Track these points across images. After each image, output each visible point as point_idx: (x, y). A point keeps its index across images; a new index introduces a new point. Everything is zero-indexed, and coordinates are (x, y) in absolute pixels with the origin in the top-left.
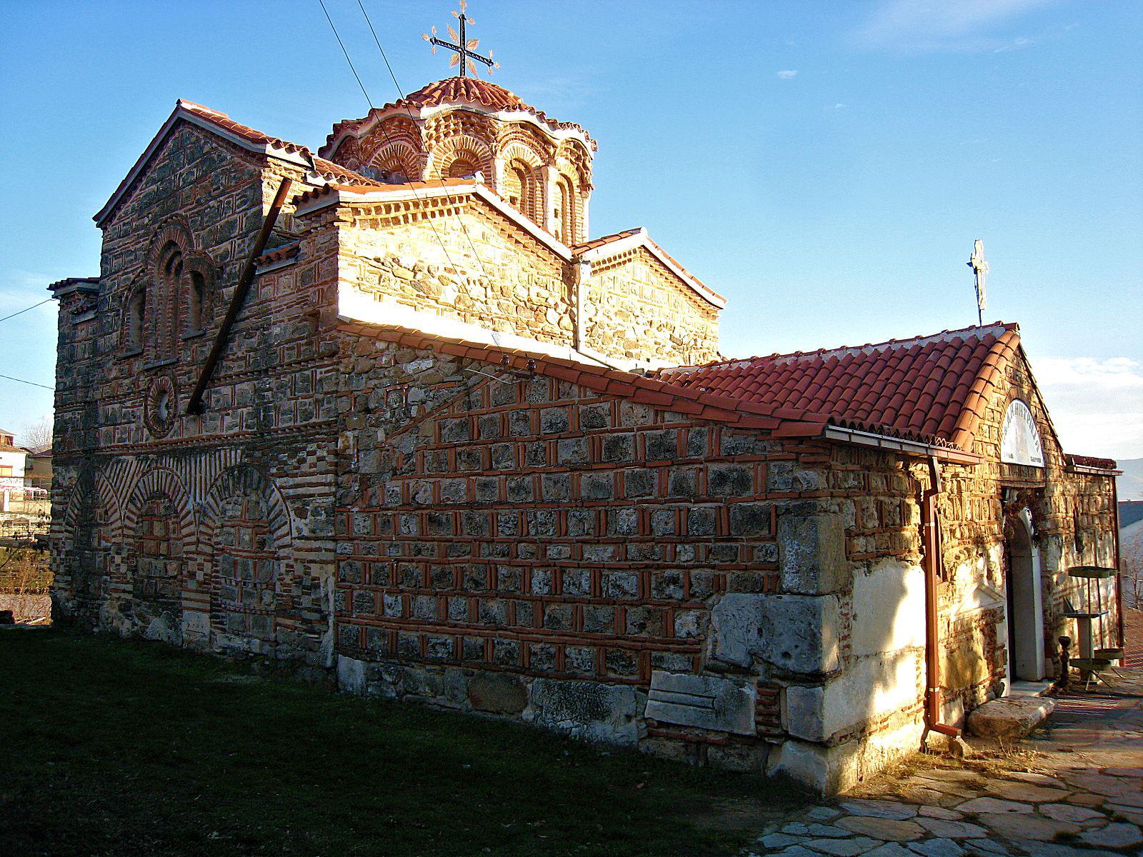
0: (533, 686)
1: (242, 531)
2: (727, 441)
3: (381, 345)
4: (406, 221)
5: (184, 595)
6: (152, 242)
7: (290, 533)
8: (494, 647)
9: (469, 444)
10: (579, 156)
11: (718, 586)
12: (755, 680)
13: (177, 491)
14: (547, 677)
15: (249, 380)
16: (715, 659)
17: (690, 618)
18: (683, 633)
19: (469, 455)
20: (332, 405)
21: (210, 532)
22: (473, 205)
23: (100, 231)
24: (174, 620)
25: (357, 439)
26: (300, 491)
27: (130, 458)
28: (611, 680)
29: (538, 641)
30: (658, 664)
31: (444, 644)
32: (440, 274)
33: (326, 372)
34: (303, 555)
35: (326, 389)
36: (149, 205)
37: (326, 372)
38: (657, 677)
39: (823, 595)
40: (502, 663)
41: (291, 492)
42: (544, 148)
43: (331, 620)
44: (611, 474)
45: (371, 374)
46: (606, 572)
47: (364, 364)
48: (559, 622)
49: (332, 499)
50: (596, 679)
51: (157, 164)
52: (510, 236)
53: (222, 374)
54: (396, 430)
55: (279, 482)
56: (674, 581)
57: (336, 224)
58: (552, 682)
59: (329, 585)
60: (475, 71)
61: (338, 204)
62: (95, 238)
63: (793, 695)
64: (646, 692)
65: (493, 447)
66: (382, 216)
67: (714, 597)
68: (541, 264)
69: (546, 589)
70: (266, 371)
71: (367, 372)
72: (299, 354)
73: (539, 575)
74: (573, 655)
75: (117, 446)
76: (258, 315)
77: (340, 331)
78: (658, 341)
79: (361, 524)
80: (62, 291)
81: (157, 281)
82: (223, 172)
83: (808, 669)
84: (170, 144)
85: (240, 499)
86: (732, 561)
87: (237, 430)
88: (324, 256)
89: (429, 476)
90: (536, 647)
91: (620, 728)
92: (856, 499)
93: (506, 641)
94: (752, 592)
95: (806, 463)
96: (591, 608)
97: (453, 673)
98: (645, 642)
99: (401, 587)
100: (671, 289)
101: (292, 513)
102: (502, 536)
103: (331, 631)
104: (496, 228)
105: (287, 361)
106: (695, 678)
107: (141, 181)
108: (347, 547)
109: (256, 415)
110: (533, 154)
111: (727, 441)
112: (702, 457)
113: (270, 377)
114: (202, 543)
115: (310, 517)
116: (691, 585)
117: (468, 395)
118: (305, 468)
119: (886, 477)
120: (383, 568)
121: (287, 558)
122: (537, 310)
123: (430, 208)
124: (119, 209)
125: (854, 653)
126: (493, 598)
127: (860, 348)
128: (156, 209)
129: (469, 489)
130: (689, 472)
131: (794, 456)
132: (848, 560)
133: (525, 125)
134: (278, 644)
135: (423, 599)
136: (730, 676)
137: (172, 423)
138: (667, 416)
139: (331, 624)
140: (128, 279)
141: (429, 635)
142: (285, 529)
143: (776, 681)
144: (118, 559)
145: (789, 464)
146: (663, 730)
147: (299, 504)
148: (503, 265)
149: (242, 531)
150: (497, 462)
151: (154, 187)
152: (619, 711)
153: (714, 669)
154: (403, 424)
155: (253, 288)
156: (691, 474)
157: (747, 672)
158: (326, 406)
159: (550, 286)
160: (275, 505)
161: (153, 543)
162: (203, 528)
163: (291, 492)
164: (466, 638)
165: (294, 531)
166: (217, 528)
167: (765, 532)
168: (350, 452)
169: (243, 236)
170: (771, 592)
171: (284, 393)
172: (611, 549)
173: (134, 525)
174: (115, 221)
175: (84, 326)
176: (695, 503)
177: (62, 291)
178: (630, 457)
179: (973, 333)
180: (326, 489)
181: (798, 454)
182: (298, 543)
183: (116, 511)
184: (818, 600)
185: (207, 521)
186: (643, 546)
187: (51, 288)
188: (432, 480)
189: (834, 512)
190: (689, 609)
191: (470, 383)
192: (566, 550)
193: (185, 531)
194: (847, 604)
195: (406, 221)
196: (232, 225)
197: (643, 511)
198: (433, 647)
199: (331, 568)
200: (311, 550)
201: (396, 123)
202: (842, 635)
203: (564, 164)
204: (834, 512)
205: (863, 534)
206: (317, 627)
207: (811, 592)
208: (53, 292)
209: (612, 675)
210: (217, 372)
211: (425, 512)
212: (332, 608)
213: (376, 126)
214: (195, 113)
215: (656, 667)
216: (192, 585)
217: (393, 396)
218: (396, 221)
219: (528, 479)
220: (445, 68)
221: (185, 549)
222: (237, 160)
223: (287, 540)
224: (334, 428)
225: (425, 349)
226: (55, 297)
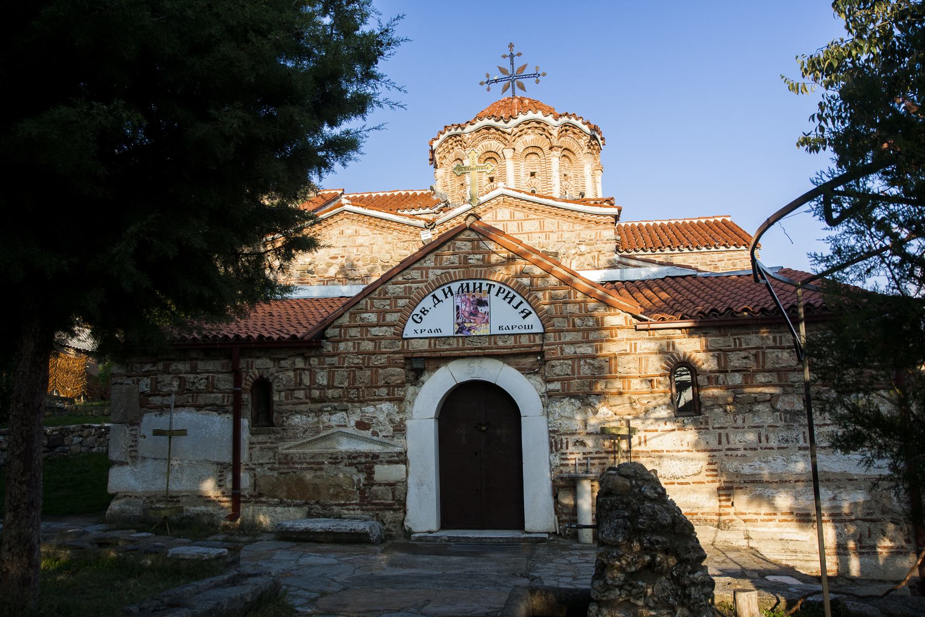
148: (371, 244)
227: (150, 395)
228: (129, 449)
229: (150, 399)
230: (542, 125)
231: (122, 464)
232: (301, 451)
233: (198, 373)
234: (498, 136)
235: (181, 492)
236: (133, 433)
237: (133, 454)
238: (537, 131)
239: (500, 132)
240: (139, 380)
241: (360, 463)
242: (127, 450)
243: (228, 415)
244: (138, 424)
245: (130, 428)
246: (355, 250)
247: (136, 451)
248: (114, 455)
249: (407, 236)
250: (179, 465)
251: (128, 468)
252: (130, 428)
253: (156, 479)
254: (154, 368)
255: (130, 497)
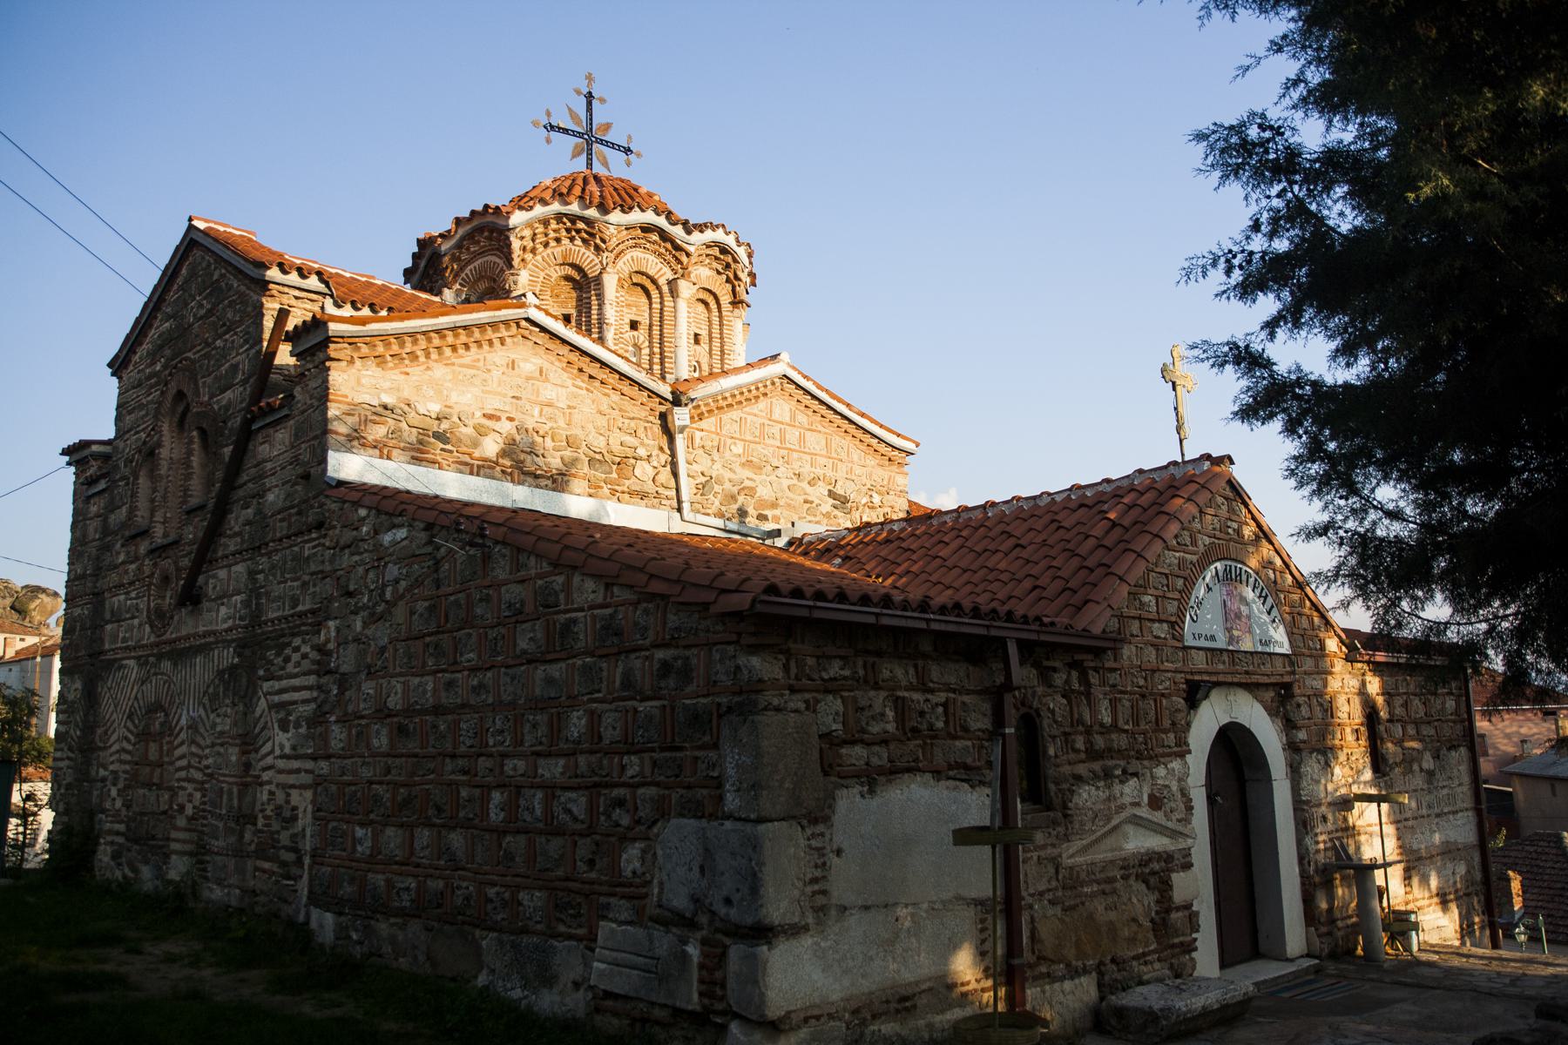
0: (488, 941)
1: (230, 750)
2: (673, 620)
3: (363, 512)
4: (428, 356)
5: (174, 835)
6: (163, 393)
7: (272, 752)
8: (453, 892)
9: (437, 633)
10: (728, 266)
11: (662, 812)
12: (699, 935)
13: (171, 703)
14: (500, 931)
15: (244, 561)
16: (660, 906)
17: (635, 851)
18: (628, 873)
19: (437, 646)
20: (318, 589)
21: (200, 752)
22: (526, 333)
23: (115, 380)
24: (161, 868)
25: (338, 630)
26: (286, 697)
27: (132, 663)
28: (560, 935)
29: (494, 884)
30: (603, 913)
31: (407, 889)
32: (476, 421)
33: (314, 547)
34: (282, 778)
35: (313, 568)
36: (161, 347)
37: (314, 547)
38: (605, 928)
39: (771, 821)
40: (459, 914)
41: (276, 698)
42: (674, 256)
43: (307, 861)
44: (563, 665)
45: (352, 548)
46: (558, 792)
47: (349, 535)
48: (513, 859)
49: (313, 706)
50: (544, 934)
51: (172, 296)
52: (581, 370)
53: (220, 554)
54: (374, 618)
55: (266, 686)
56: (620, 803)
57: (328, 364)
58: (505, 937)
59: (305, 821)
60: (615, 167)
61: (328, 340)
62: (109, 389)
63: (736, 952)
64: (593, 950)
65: (458, 634)
66: (408, 350)
67: (659, 824)
68: (627, 405)
69: (502, 815)
70: (259, 547)
71: (349, 546)
72: (290, 526)
73: (497, 796)
74: (525, 903)
75: (120, 648)
76: (255, 479)
77: (327, 496)
78: (810, 499)
79: (338, 736)
80: (77, 457)
81: (166, 440)
82: (231, 304)
83: (749, 920)
84: (184, 271)
85: (229, 710)
86: (677, 776)
87: (230, 623)
88: (316, 404)
89: (401, 675)
90: (491, 892)
91: (568, 1000)
92: (845, 694)
93: (465, 884)
94: (695, 817)
95: (749, 646)
96: (543, 839)
97: (415, 926)
98: (593, 883)
99: (372, 816)
100: (831, 429)
101: (276, 726)
102: (463, 749)
103: (306, 877)
104: (560, 361)
105: (278, 535)
106: (639, 932)
107: (156, 318)
108: (324, 766)
109: (246, 604)
110: (660, 265)
111: (673, 620)
112: (647, 642)
113: (262, 555)
114: (193, 767)
115: (292, 731)
116: (636, 809)
117: (436, 571)
118: (290, 668)
119: (916, 666)
120: (355, 792)
121: (269, 782)
122: (623, 463)
123: (463, 338)
124: (135, 353)
125: (834, 901)
126: (453, 828)
127: (1034, 498)
128: (168, 352)
129: (435, 690)
130: (636, 662)
131: (734, 637)
132: (826, 774)
133: (647, 229)
134: (257, 895)
135: (390, 831)
136: (674, 930)
137: (172, 617)
138: (616, 590)
139: (306, 867)
140: (139, 439)
141: (396, 878)
142: (268, 747)
143: (719, 936)
144: (114, 792)
145: (731, 649)
146: (609, 1003)
147: (282, 715)
148: (569, 407)
149: (230, 750)
150: (461, 655)
151: (167, 324)
152: (568, 975)
153: (656, 920)
154: (379, 609)
155: (251, 447)
156: (638, 664)
157: (691, 924)
158: (312, 590)
159: (641, 433)
160: (261, 716)
161: (148, 769)
162: (194, 749)
163: (276, 698)
164: (429, 882)
165: (277, 748)
166: (207, 747)
167: (707, 738)
168: (331, 646)
169: (244, 382)
170: (712, 817)
171: (274, 575)
172: (562, 762)
173: (130, 748)
174: (131, 368)
175: (96, 499)
176: (642, 700)
177: (77, 457)
178: (580, 645)
179: (1172, 469)
180: (305, 694)
181: (739, 634)
182: (281, 764)
183: (114, 731)
184: (762, 828)
185: (199, 739)
186: (593, 758)
187: (65, 452)
188: (402, 679)
189: (796, 711)
190: (635, 840)
191: (439, 556)
192: (521, 765)
193: (178, 752)
194: (822, 835)
195: (428, 356)
196: (235, 367)
197: (592, 713)
198: (398, 893)
199: (309, 794)
200: (290, 772)
201: (486, 234)
202: (809, 876)
203: (704, 273)
204: (796, 711)
205: (862, 741)
206: (294, 871)
207: (752, 816)
208: (67, 458)
209: (562, 928)
210: (215, 551)
211: (395, 719)
212: (308, 848)
213: (463, 239)
214: (205, 233)
215: (604, 918)
216: (181, 822)
217: (371, 575)
218: (413, 356)
219: (489, 674)
220: (562, 160)
221: (178, 775)
222: (243, 288)
223: (269, 760)
224: (318, 617)
225: (400, 515)
226: (69, 464)
227: (845, 742)
228: (809, 889)
229: (844, 751)
230: (729, 259)
231: (795, 931)
232: (1088, 858)
233: (932, 691)
234: (663, 251)
235: (917, 983)
236: (813, 843)
237: (821, 900)
238: (715, 265)
239: (669, 246)
240: (817, 701)
241: (1153, 873)
242: (803, 893)
243: (988, 791)
244: (826, 820)
245: (809, 832)
246: (536, 412)
247: (824, 892)
248: (778, 907)
249: (635, 409)
250: (913, 915)
251: (807, 941)
252: (809, 832)
253: (871, 959)
254: (847, 673)
255: (818, 1018)
